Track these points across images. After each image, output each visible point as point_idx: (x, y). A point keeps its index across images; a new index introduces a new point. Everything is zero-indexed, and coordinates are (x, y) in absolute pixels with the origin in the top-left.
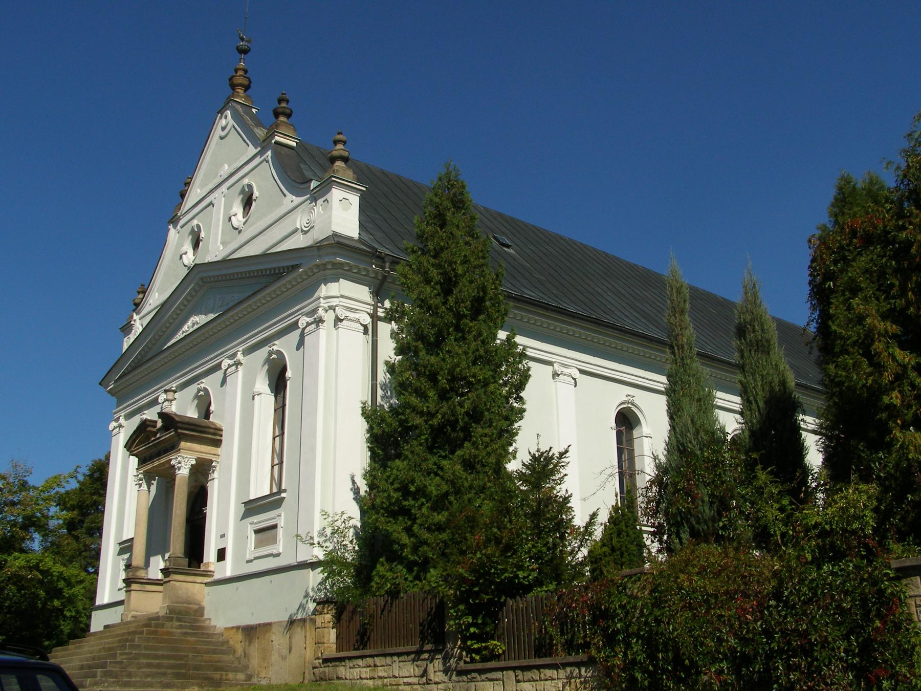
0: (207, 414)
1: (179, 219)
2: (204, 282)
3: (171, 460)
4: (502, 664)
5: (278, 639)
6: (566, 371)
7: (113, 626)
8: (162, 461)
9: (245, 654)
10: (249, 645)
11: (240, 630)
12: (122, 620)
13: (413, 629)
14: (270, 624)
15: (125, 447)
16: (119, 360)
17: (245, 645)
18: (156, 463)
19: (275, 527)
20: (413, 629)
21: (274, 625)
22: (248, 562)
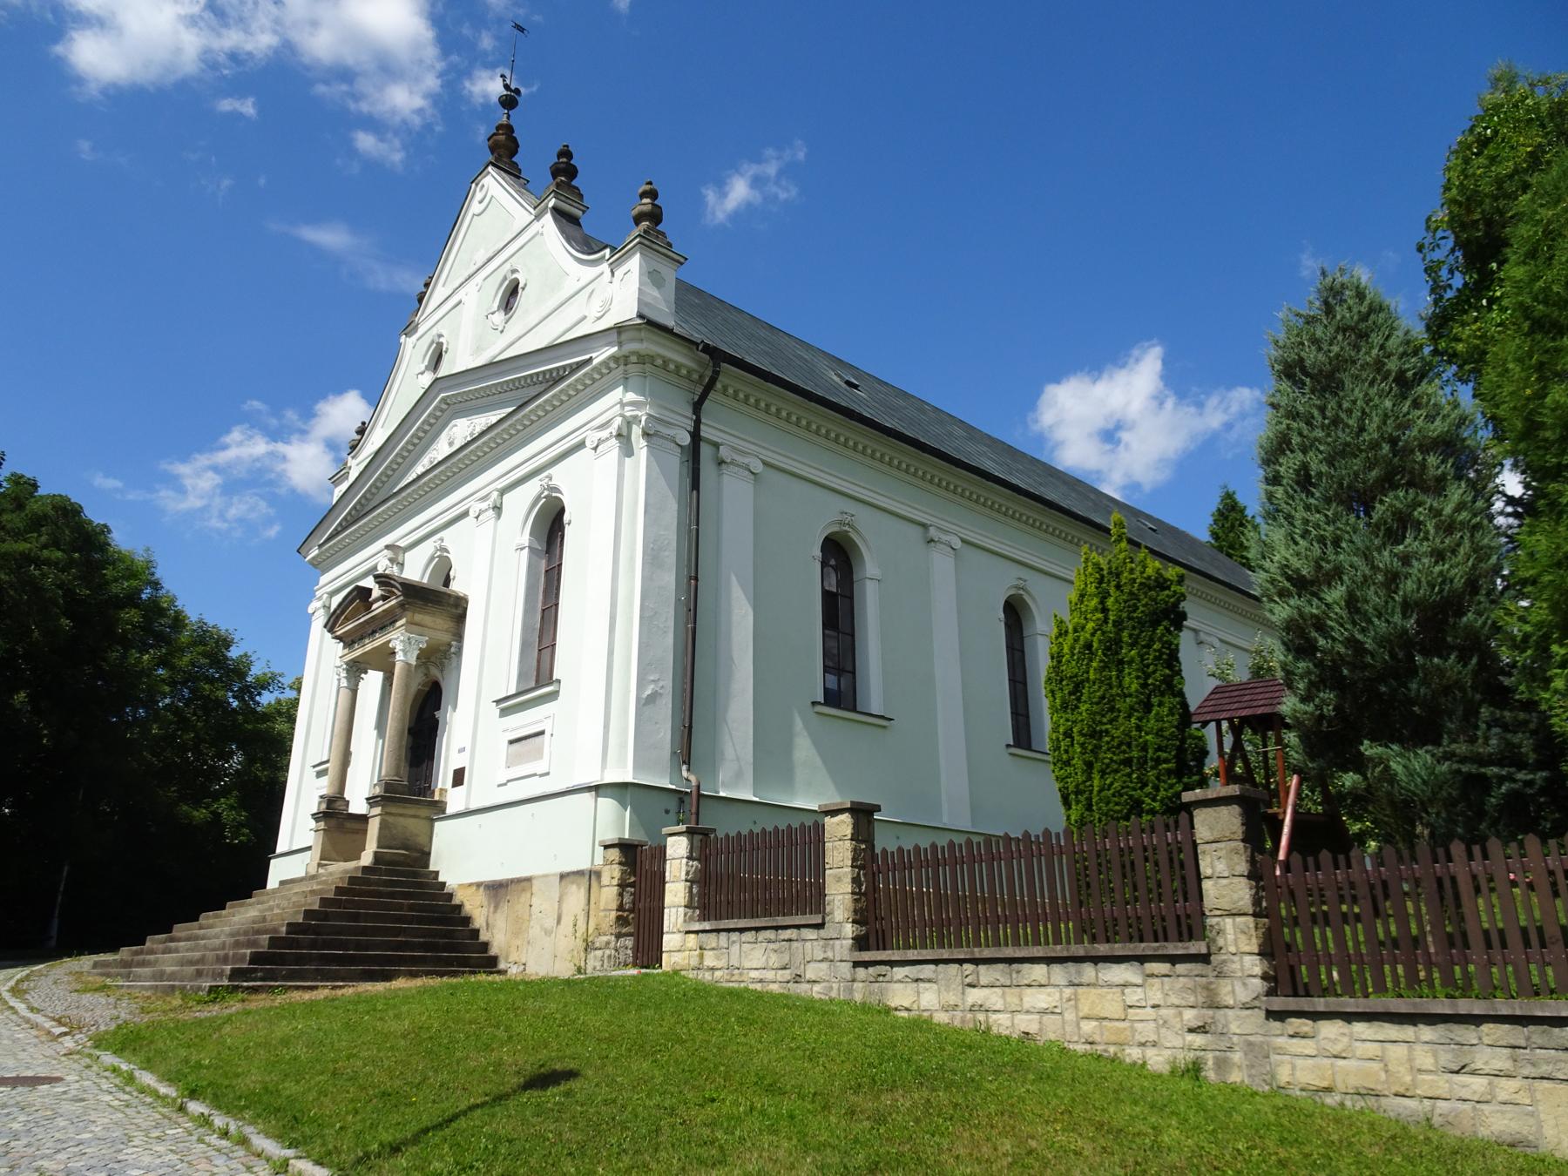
0: (447, 582)
1: (416, 329)
2: (448, 404)
3: (389, 641)
4: (1320, 1004)
5: (542, 902)
6: (945, 538)
7: (292, 881)
8: (377, 643)
9: (488, 924)
10: (495, 911)
11: (482, 889)
12: (307, 873)
13: (1380, 897)
14: (529, 880)
15: (325, 627)
16: (325, 517)
17: (488, 911)
18: (368, 647)
19: (542, 733)
20: (1380, 897)
21: (534, 882)
22: (499, 786)
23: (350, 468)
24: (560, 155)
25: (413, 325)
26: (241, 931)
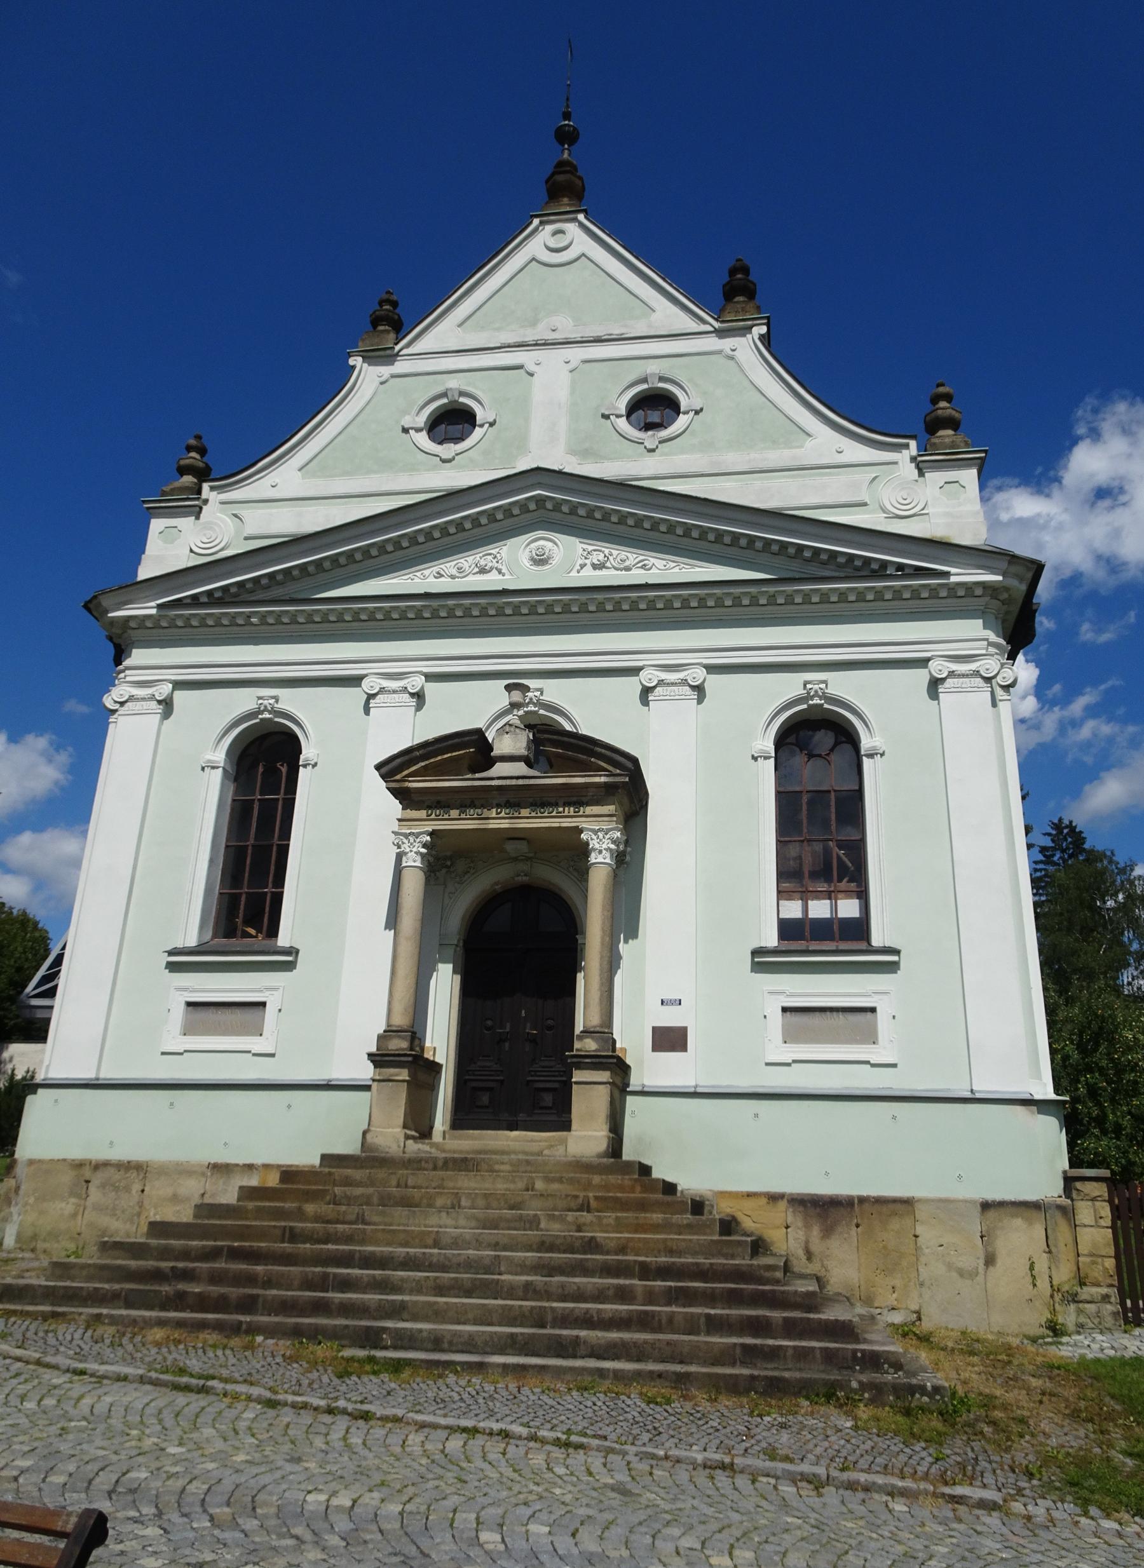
14: (908, 1202)
21: (918, 1206)
23: (206, 501)
24: (733, 272)
25: (388, 352)
26: (577, 1244)
